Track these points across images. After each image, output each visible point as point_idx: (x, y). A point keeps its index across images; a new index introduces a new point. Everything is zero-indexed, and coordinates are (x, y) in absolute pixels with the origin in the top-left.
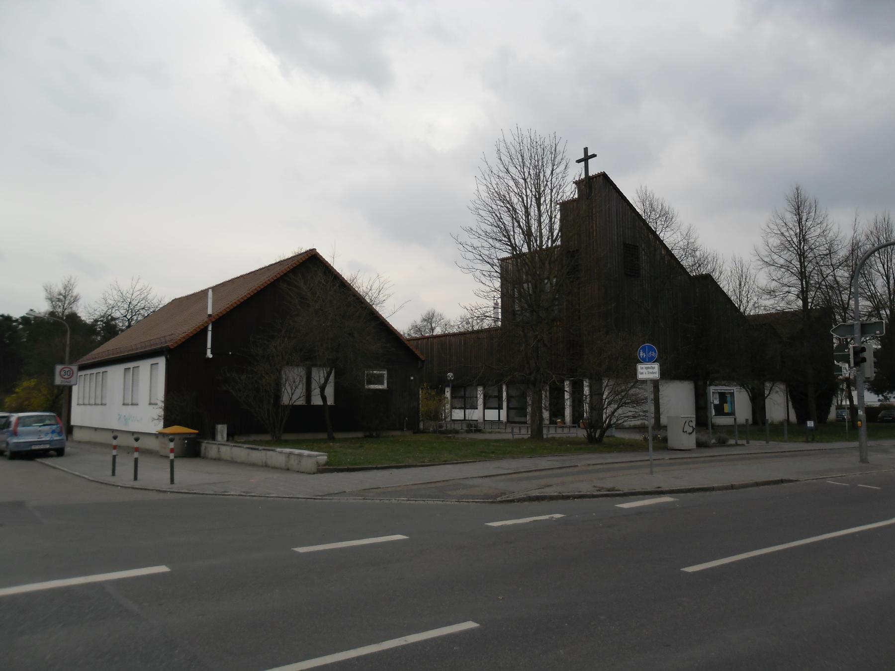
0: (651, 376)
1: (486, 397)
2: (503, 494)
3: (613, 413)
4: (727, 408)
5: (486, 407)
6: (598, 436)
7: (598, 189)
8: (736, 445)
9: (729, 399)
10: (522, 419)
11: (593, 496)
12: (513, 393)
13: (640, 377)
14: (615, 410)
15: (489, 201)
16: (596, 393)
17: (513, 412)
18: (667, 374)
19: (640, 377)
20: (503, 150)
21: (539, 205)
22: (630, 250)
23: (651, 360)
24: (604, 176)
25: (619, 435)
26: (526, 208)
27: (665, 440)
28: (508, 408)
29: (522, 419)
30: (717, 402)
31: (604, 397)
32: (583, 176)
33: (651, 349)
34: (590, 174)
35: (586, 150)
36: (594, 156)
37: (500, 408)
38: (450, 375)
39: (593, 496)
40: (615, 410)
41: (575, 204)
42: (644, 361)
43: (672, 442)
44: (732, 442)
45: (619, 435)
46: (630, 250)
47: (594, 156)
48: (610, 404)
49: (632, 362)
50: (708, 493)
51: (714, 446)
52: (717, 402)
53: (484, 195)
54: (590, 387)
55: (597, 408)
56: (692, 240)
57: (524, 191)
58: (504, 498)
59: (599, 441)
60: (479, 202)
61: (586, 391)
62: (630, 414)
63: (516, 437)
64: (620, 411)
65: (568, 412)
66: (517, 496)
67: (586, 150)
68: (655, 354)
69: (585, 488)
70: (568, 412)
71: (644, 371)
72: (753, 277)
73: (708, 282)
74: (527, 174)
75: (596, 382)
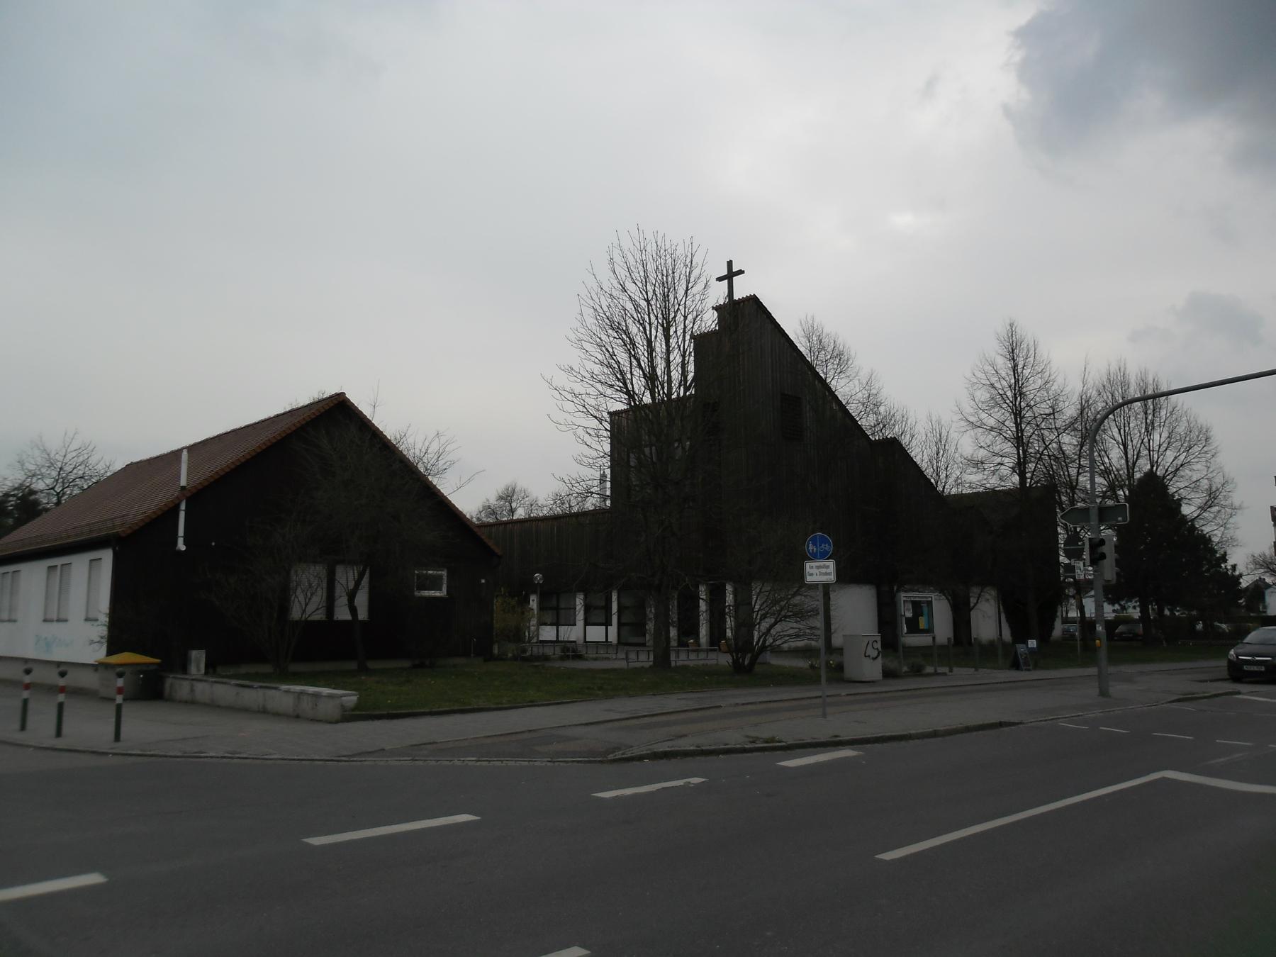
0: (824, 579)
1: (587, 609)
2: (614, 750)
3: (769, 630)
4: (923, 623)
5: (587, 623)
6: (748, 666)
8: (936, 674)
9: (925, 610)
10: (639, 640)
11: (745, 751)
14: (772, 626)
16: (743, 603)
19: (809, 579)
20: (618, 259)
23: (823, 556)
24: (753, 301)
26: (649, 342)
27: (840, 667)
28: (620, 624)
29: (639, 640)
30: (909, 614)
31: (757, 607)
33: (824, 541)
34: (736, 297)
35: (730, 264)
37: (607, 623)
39: (745, 751)
40: (772, 626)
42: (814, 557)
43: (850, 672)
44: (929, 669)
48: (764, 617)
49: (797, 560)
51: (906, 675)
52: (909, 614)
53: (590, 321)
54: (735, 594)
55: (745, 625)
58: (618, 755)
59: (749, 670)
60: (583, 331)
61: (730, 599)
62: (792, 632)
64: (778, 627)
65: (703, 631)
67: (730, 264)
68: (829, 548)
69: (734, 738)
70: (703, 631)
71: (815, 571)
73: (893, 450)
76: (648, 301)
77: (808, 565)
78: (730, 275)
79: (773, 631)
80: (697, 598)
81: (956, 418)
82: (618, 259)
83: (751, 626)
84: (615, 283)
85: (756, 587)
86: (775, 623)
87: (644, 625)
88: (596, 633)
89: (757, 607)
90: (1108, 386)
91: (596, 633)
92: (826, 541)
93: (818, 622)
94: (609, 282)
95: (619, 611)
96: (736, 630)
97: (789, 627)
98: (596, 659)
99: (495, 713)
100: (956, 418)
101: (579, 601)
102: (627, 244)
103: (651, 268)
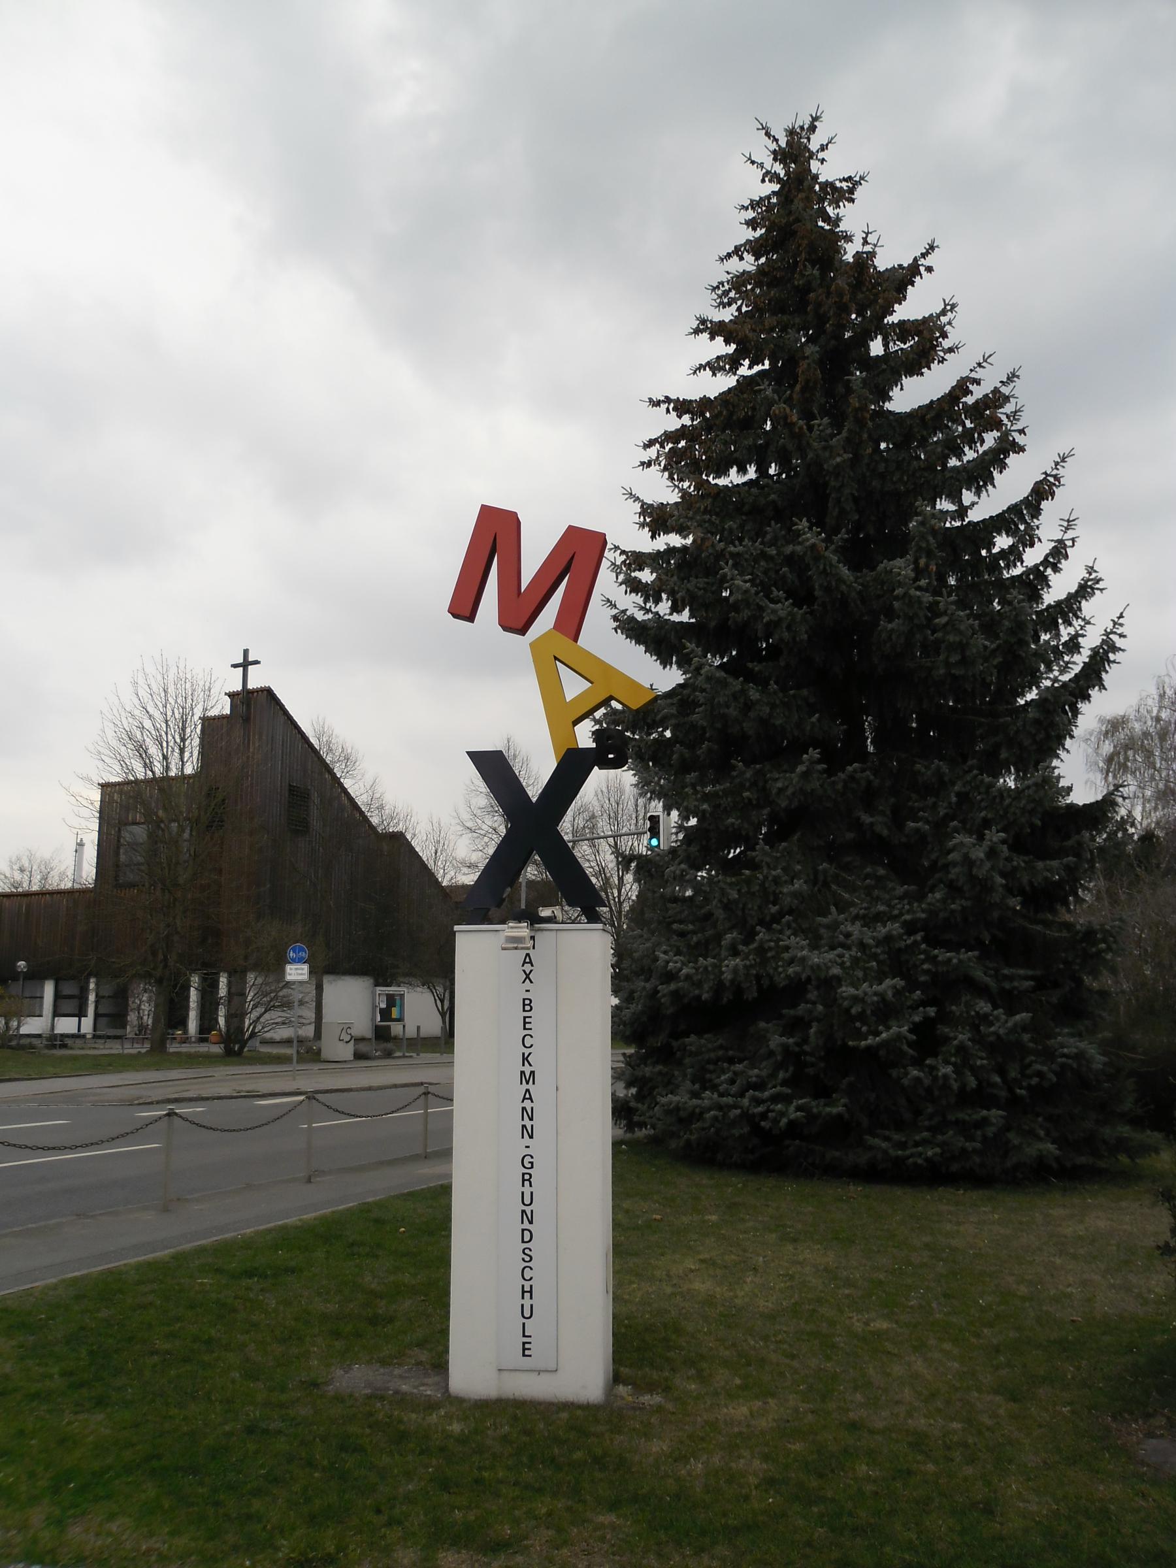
0: (300, 978)
1: (58, 996)
2: (138, 1099)
3: (259, 1018)
4: (395, 1013)
5: (57, 1013)
6: (236, 1046)
7: (257, 708)
8: (404, 1057)
9: (398, 1002)
10: (118, 1032)
11: (232, 1097)
12: (107, 991)
13: (289, 978)
14: (261, 1016)
15: (114, 743)
16: (238, 993)
17: (103, 1021)
18: (323, 969)
19: (289, 978)
20: (141, 681)
21: (182, 751)
22: (297, 796)
23: (300, 961)
24: (268, 693)
25: (265, 1049)
26: (165, 757)
27: (319, 1051)
28: (97, 1016)
29: (118, 1032)
30: (383, 1006)
31: (249, 998)
32: (240, 688)
33: (301, 950)
34: (250, 686)
35: (246, 652)
36: (257, 662)
37: (81, 1013)
38: (22, 964)
39: (232, 1097)
40: (261, 1016)
41: (225, 721)
42: (294, 961)
43: (325, 1055)
44: (398, 1054)
45: (265, 1049)
46: (297, 796)
47: (257, 662)
48: (255, 1007)
49: (281, 962)
50: (345, 1094)
51: (379, 1058)
52: (383, 1006)
53: (110, 734)
54: (229, 985)
55: (236, 1016)
56: (377, 795)
57: (164, 736)
58: (141, 1101)
59: (239, 1053)
60: (102, 744)
61: (223, 991)
62: (279, 1020)
63: (126, 1051)
64: (267, 1016)
65: (193, 1025)
66: (155, 1099)
67: (246, 652)
68: (305, 955)
69: (225, 1091)
70: (193, 1025)
71: (293, 972)
72: (452, 844)
73: (398, 840)
74: (169, 713)
75: (237, 975)
76: (167, 722)
77: (288, 967)
78: (245, 664)
79: (262, 1020)
80: (186, 988)
81: (454, 822)
82: (141, 681)
83: (242, 1015)
84: (136, 702)
85: (251, 977)
86: (265, 1012)
87: (125, 1015)
88: (67, 1025)
89: (249, 998)
90: (605, 790)
91: (67, 1025)
92: (303, 950)
93: (310, 1014)
94: (130, 701)
95: (97, 1002)
96: (228, 1018)
97: (274, 1016)
98: (83, 1049)
99: (17, 1083)
100: (454, 822)
101: (49, 989)
102: (151, 669)
103: (171, 690)
